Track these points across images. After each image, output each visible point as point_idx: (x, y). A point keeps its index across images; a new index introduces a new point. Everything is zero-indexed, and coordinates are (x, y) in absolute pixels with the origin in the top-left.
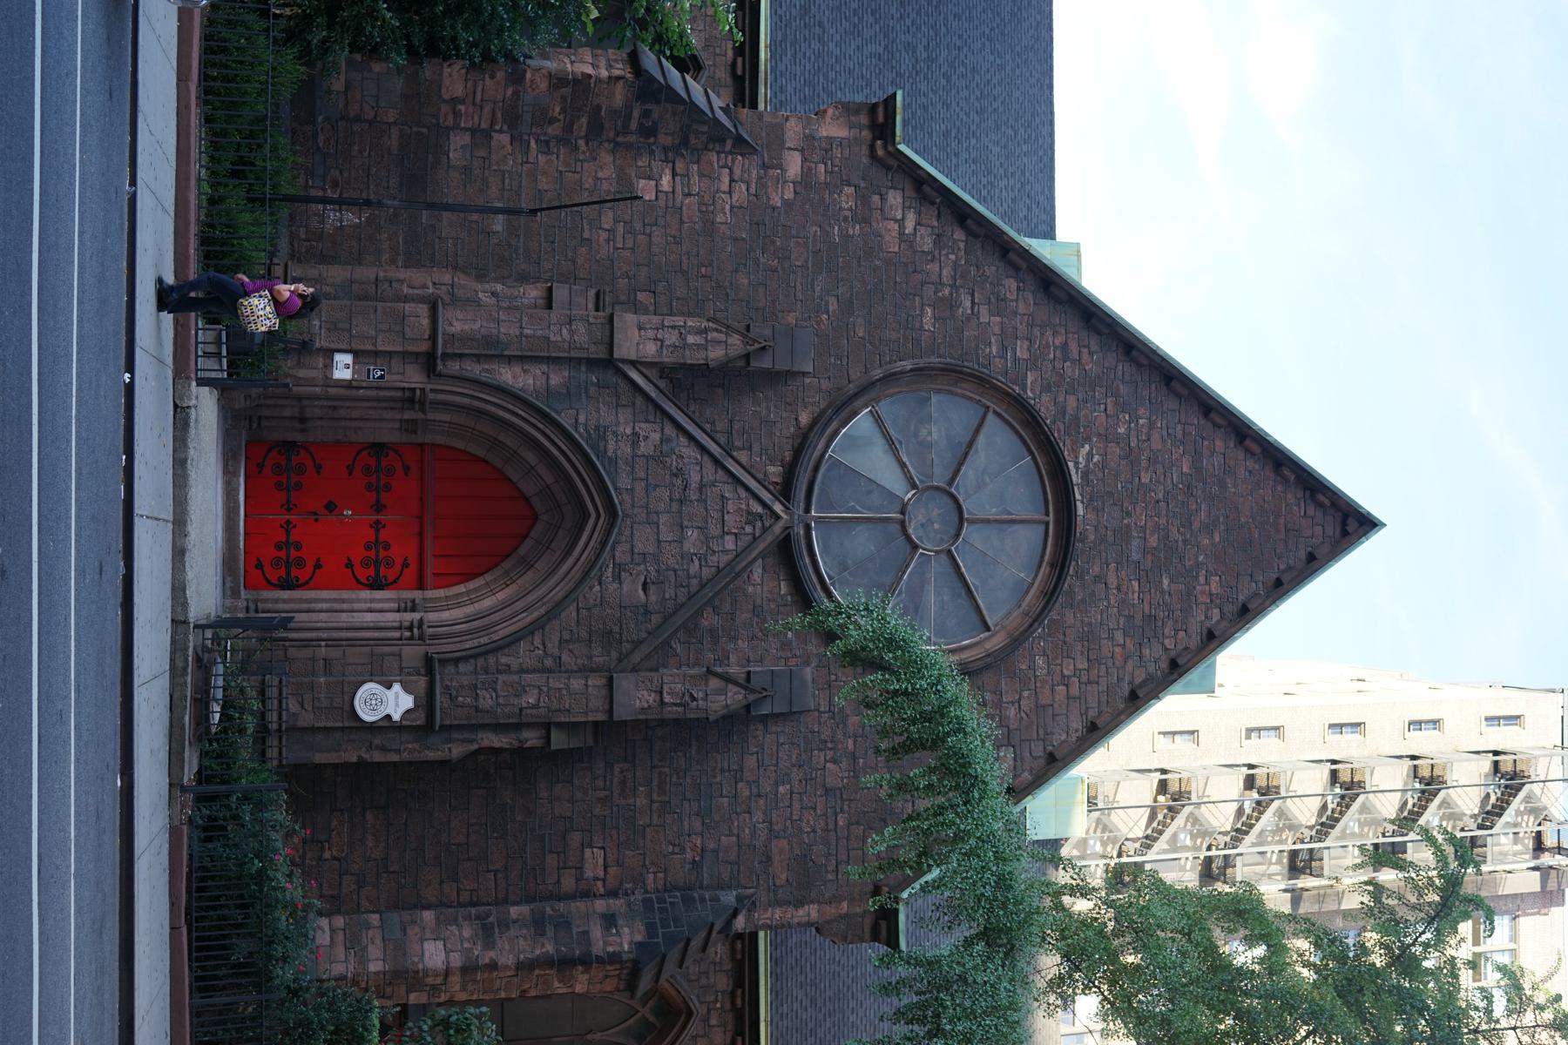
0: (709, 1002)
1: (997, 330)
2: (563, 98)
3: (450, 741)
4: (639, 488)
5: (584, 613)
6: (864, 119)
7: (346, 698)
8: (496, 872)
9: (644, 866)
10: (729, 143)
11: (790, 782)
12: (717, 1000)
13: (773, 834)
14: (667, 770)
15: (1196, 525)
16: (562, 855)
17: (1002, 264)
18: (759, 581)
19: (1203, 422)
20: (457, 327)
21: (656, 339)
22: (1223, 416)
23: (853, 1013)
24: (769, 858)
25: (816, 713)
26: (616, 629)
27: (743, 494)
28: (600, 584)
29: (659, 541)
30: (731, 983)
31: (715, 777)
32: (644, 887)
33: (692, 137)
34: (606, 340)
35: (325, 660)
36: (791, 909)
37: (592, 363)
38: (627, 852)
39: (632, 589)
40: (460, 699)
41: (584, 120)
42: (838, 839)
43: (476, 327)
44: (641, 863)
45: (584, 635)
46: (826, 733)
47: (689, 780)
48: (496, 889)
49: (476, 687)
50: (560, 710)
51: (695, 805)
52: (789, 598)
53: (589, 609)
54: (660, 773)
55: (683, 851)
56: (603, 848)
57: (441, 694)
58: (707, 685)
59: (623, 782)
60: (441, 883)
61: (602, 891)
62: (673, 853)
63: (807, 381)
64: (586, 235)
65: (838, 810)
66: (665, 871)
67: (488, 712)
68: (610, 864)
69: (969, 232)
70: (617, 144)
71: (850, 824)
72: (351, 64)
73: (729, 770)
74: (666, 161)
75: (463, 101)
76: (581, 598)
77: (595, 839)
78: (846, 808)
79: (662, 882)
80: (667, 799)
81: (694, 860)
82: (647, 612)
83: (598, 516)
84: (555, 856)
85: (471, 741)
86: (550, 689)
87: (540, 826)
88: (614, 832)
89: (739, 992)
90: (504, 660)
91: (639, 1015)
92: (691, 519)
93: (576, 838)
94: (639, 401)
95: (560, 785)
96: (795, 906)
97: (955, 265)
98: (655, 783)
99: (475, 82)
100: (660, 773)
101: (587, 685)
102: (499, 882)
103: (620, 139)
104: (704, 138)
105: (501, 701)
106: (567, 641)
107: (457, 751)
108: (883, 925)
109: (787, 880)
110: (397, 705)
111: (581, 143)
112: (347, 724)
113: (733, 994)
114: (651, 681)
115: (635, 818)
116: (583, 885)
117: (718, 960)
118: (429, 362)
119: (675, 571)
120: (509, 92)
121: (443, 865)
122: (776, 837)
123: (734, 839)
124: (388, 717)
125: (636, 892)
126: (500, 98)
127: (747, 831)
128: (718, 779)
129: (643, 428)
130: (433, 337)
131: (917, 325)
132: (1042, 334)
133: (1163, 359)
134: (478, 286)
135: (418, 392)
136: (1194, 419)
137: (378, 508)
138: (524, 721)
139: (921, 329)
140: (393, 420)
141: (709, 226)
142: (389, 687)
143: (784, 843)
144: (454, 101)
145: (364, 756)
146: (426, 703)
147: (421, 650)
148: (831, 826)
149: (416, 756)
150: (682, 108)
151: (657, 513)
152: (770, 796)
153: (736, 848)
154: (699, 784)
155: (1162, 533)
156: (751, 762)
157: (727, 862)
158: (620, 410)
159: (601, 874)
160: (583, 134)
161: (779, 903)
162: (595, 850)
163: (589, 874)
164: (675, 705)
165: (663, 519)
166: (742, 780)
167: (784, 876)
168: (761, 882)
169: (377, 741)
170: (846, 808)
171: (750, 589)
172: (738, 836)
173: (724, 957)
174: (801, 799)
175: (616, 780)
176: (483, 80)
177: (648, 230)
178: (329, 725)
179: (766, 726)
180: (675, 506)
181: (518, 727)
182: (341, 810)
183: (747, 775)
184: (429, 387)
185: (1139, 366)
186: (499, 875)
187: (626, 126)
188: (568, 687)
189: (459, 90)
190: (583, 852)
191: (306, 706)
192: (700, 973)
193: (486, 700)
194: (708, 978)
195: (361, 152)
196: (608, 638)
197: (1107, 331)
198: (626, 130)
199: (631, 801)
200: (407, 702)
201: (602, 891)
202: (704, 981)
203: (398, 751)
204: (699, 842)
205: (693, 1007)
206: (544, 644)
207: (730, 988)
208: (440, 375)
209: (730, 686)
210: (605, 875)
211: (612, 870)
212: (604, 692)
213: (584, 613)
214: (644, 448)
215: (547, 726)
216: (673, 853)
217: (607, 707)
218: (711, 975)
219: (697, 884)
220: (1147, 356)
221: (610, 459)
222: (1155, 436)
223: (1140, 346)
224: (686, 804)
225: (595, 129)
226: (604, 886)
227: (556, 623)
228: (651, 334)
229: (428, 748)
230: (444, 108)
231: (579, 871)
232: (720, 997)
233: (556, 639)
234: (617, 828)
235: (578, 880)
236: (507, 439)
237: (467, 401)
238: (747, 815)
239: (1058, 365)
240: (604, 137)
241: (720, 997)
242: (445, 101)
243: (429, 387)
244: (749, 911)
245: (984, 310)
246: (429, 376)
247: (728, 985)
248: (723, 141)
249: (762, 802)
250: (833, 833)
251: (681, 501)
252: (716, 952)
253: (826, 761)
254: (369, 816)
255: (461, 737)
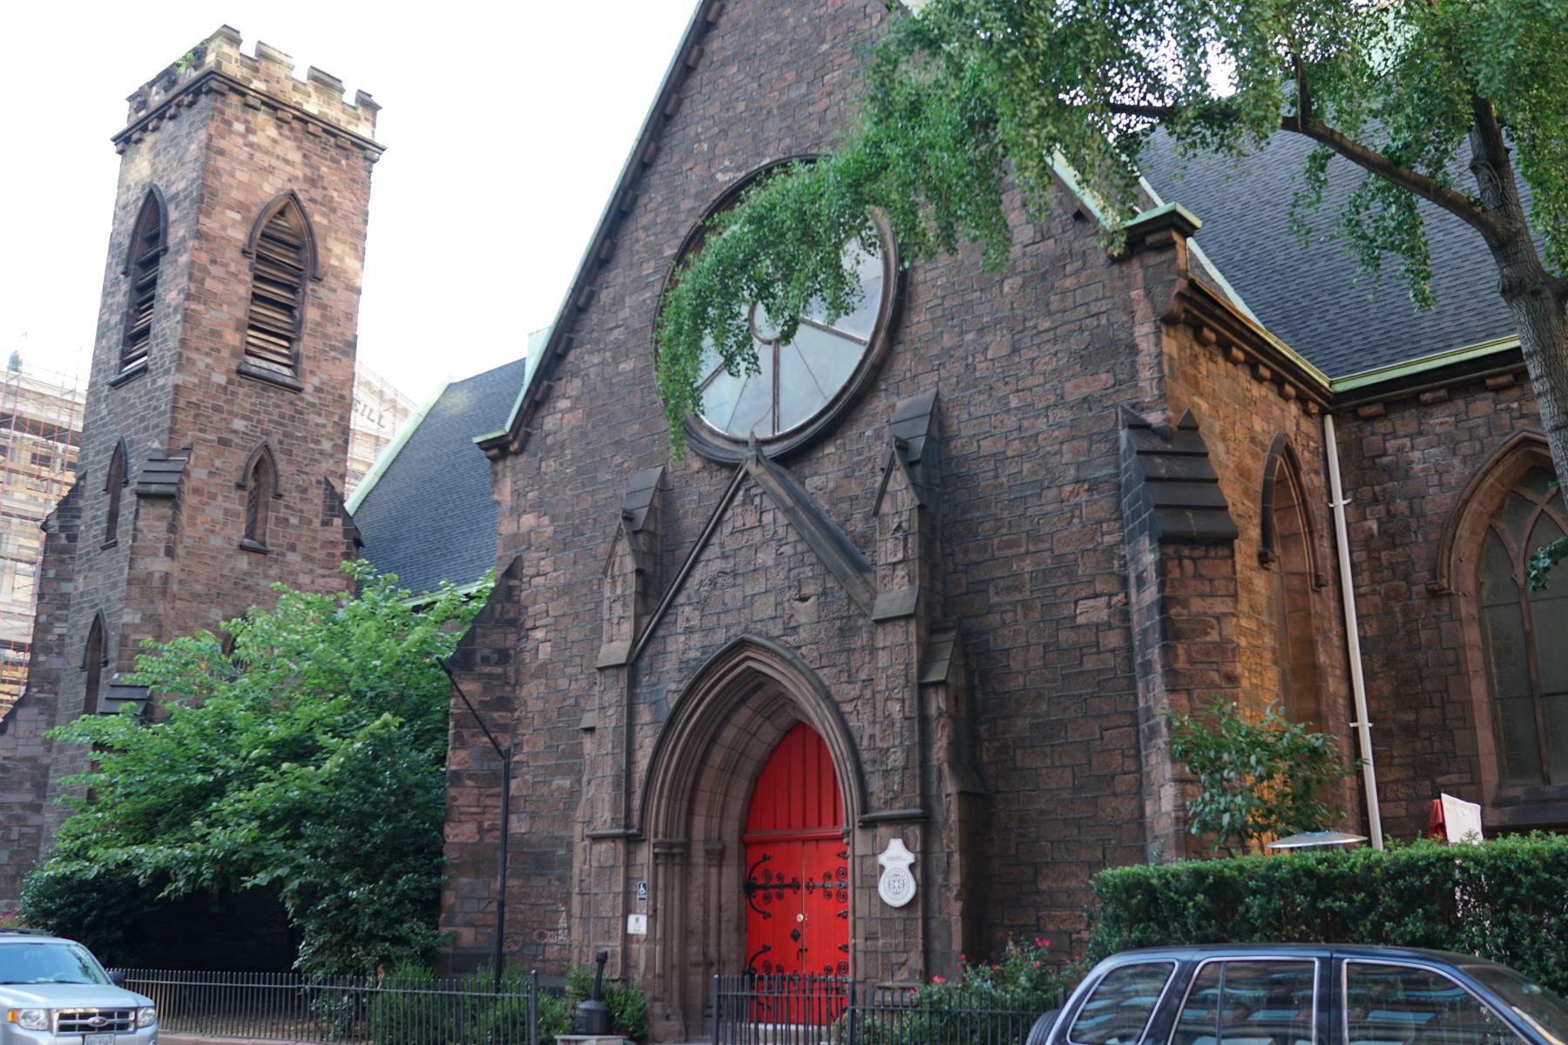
0: (1512, 418)
1: (634, 297)
2: (473, 735)
3: (939, 796)
4: (726, 619)
5: (825, 661)
6: (500, 467)
7: (896, 915)
8: (1103, 729)
9: (1094, 550)
10: (512, 582)
11: (1006, 396)
12: (1508, 408)
13: (1060, 402)
14: (996, 541)
15: (779, 38)
16: (1085, 650)
17: (591, 310)
18: (824, 478)
19: (700, 69)
20: (607, 815)
21: (618, 624)
22: (689, 53)
23: (212, 349)
24: (1085, 400)
25: (941, 384)
26: (838, 623)
27: (729, 513)
28: (800, 647)
29: (766, 592)
30: (1482, 395)
31: (1002, 484)
32: (1117, 544)
33: (507, 617)
34: (614, 672)
35: (866, 939)
36: (1140, 359)
37: (633, 683)
38: (1080, 572)
39: (805, 613)
40: (895, 788)
41: (496, 715)
42: (1065, 323)
43: (606, 797)
44: (1092, 553)
45: (843, 658)
46: (958, 368)
47: (1005, 514)
48: (1121, 727)
49: (887, 771)
50: (906, 675)
51: (1030, 501)
52: (839, 442)
53: (821, 656)
54: (999, 549)
55: (1078, 506)
56: (1076, 603)
57: (891, 809)
58: (887, 515)
59: (1008, 590)
60: (1115, 795)
61: (1121, 596)
62: (1080, 517)
63: (670, 469)
64: (572, 701)
65: (1034, 332)
66: (1100, 522)
67: (908, 756)
68: (1092, 591)
69: (569, 347)
70: (516, 683)
71: (1050, 314)
72: (449, 923)
73: (996, 469)
74: (527, 637)
75: (480, 824)
76: (813, 666)
77: (1066, 613)
78: (1032, 323)
79: (1112, 524)
80: (1024, 535)
81: (1089, 490)
82: (824, 594)
83: (748, 658)
84: (1085, 659)
85: (940, 771)
86: (887, 689)
87: (1054, 681)
88: (1060, 591)
89: (1489, 382)
90: (865, 742)
91: (1547, 508)
92: (749, 562)
93: (1066, 637)
94: (661, 632)
95: (1012, 663)
96: (1137, 355)
97: (591, 353)
98: (1009, 553)
99: (461, 814)
100: (999, 549)
101: (884, 648)
102: (1112, 724)
103: (513, 681)
104: (508, 606)
105: (897, 742)
106: (849, 676)
107: (950, 787)
108: (1150, 240)
109: (1108, 371)
110: (898, 858)
111: (517, 714)
112: (920, 914)
113: (1497, 389)
114: (884, 577)
115: (1044, 570)
116: (1116, 622)
117: (1451, 420)
118: (632, 840)
119: (790, 570)
120: (470, 783)
121: (1096, 793)
122: (1062, 398)
123: (1065, 447)
124: (912, 867)
125: (1122, 553)
126: (476, 791)
127: (1056, 433)
128: (1004, 480)
129: (681, 625)
130: (612, 838)
131: (631, 375)
132: (638, 252)
133: (646, 130)
134: (584, 798)
135: (657, 850)
136: (696, 80)
137: (796, 886)
138: (916, 714)
139: (633, 370)
140: (707, 875)
141: (567, 589)
142: (882, 868)
143: (1069, 386)
144: (481, 831)
145: (955, 893)
146: (898, 823)
147: (858, 833)
148: (1051, 335)
149: (955, 834)
150: (479, 630)
151: (744, 598)
152: (1020, 416)
153: (1075, 443)
154: (1010, 500)
155: (785, 70)
156: (987, 446)
157: (1089, 450)
158: (668, 649)
159: (1104, 600)
160: (509, 714)
161: (1134, 374)
162: (1078, 611)
163: (1104, 615)
164: (905, 546)
165: (749, 591)
166: (1004, 452)
167: (1104, 377)
168: (1110, 403)
169: (939, 879)
170: (1032, 323)
171: (831, 485)
172: (1062, 443)
173: (1448, 412)
174: (1024, 378)
175: (1007, 599)
176: (458, 806)
177: (569, 645)
178: (920, 935)
179: (953, 437)
180: (740, 580)
181: (924, 720)
182: (1038, 919)
183: (1000, 448)
184: (652, 840)
185: (658, 150)
186: (1105, 724)
187: (499, 677)
188: (886, 669)
189: (470, 828)
190: (1080, 626)
191: (902, 960)
192: (1471, 439)
193: (896, 758)
194: (1478, 427)
195: (521, 912)
196: (845, 632)
197: (631, 192)
198: (503, 677)
199: (1027, 576)
200: (896, 846)
201: (1121, 596)
202: (1482, 432)
203: (950, 855)
204: (1068, 488)
205: (1516, 439)
206: (852, 700)
207: (1491, 395)
208: (641, 829)
209: (889, 488)
210: (1105, 595)
211: (1099, 587)
212: (889, 628)
213: (825, 661)
214: (695, 622)
215: (923, 688)
216: (1080, 517)
217: (903, 623)
218: (1472, 423)
219: (1114, 480)
220: (648, 146)
221: (704, 653)
222: (711, 111)
223: (638, 156)
224: (1030, 512)
225: (505, 704)
226: (1117, 594)
227: (833, 690)
228: (615, 628)
229: (947, 820)
230: (488, 839)
231: (1101, 628)
232: (1503, 406)
233: (846, 688)
234: (1055, 588)
235: (1110, 627)
236: (717, 757)
237: (664, 802)
238: (1041, 437)
239: (659, 228)
240: (511, 695)
241: (1503, 406)
242: (481, 839)
243: (652, 840)
244: (1143, 410)
245: (621, 315)
246: (644, 840)
247: (1486, 399)
248: (511, 589)
249: (1026, 424)
250: (1058, 331)
251: (735, 576)
252: (1442, 423)
253: (986, 359)
254: (1044, 886)
255: (936, 784)
